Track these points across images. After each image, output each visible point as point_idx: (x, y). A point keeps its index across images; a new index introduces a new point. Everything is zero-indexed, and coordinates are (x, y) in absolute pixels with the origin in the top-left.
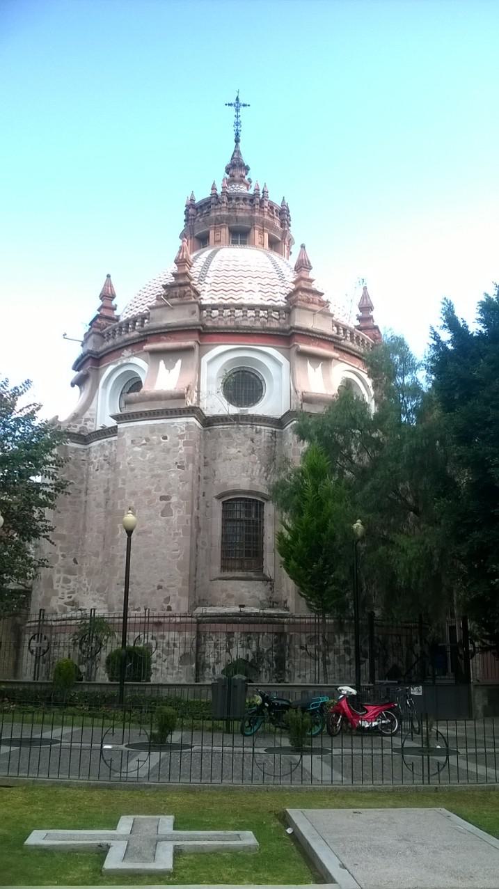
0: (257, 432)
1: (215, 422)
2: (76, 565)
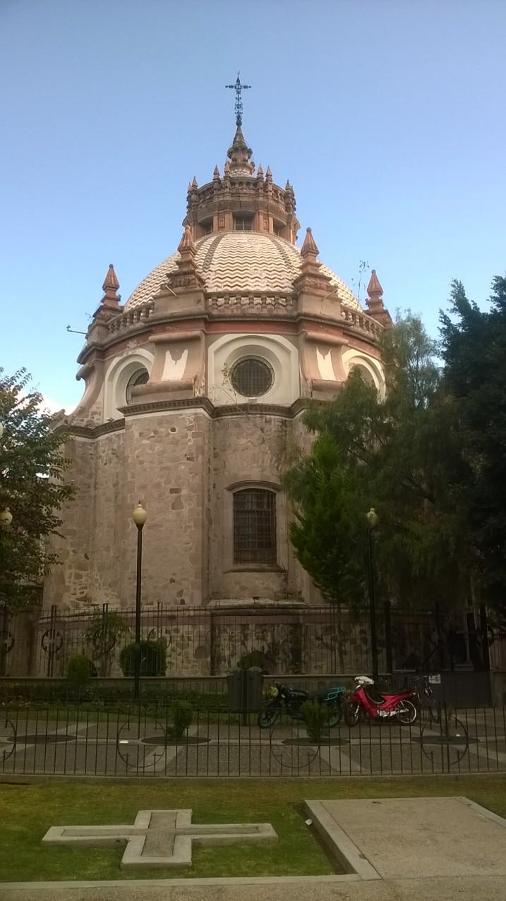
0: (266, 422)
1: (224, 412)
2: (87, 561)
